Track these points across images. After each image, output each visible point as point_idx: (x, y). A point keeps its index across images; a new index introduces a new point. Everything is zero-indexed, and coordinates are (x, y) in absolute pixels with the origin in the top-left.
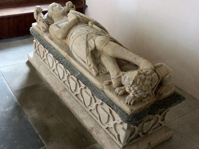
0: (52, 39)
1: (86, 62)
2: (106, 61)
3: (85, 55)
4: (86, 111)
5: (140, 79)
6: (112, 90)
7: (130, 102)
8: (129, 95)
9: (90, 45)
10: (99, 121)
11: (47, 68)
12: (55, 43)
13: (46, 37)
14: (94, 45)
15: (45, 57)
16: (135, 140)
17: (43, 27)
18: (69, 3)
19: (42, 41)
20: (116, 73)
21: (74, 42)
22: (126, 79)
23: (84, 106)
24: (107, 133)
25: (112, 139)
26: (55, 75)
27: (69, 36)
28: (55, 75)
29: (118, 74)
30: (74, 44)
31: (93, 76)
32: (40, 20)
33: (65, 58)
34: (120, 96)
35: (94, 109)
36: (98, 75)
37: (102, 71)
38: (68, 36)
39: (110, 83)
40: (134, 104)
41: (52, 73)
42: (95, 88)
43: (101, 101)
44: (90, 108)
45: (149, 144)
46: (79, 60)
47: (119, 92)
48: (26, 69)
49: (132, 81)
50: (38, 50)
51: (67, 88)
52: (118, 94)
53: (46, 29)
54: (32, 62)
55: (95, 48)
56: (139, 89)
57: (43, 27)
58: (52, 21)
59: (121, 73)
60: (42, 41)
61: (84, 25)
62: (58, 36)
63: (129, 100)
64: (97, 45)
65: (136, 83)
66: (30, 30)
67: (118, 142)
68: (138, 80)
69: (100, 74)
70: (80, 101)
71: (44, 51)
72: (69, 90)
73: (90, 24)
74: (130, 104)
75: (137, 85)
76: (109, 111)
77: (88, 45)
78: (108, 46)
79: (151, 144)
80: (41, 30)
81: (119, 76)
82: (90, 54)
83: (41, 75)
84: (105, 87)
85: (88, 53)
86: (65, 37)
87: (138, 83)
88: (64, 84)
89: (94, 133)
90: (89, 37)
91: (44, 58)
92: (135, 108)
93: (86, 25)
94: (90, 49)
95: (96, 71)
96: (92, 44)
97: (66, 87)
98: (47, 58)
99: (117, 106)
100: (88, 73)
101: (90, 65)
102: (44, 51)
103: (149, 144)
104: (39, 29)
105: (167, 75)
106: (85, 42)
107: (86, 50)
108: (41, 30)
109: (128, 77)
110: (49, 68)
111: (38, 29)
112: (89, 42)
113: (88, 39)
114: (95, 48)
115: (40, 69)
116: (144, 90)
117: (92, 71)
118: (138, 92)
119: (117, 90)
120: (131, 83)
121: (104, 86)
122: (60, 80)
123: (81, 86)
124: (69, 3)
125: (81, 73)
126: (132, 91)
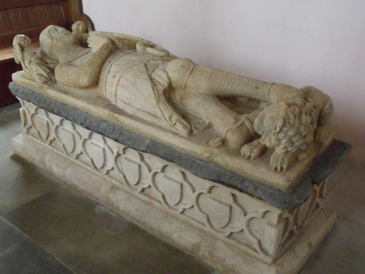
0: (66, 93)
1: (159, 114)
2: (199, 104)
3: (154, 102)
4: (172, 216)
5: (293, 113)
6: (236, 153)
7: (281, 164)
8: (274, 153)
9: (158, 82)
10: (208, 228)
11: (61, 156)
12: (77, 98)
13: (51, 93)
14: (165, 78)
15: (53, 135)
16: (288, 244)
17: (39, 74)
18: (78, 25)
19: (42, 101)
20: (231, 120)
21: (121, 83)
22: (265, 120)
23: (167, 207)
24: (232, 245)
25: (247, 254)
26: (84, 166)
27: (102, 77)
28: (84, 166)
29: (237, 120)
30: (122, 86)
31: (182, 137)
32: (30, 62)
33: (104, 121)
34: (255, 158)
35: (193, 206)
36: (191, 133)
37: (198, 126)
38: (101, 77)
39: (224, 142)
40: (289, 168)
41: (73, 163)
42: (192, 159)
43: (208, 184)
44: (181, 207)
45: (310, 244)
46: (140, 115)
47: (251, 152)
48: (16, 169)
49: (282, 120)
50: (34, 125)
51: (117, 183)
52: (250, 157)
53: (46, 76)
54: (24, 155)
55: (170, 84)
56: (296, 135)
57: (39, 74)
58: (55, 61)
59: (243, 118)
60: (42, 101)
61: (129, 52)
62: (81, 80)
63: (280, 162)
64: (174, 76)
65: (289, 123)
66: (10, 83)
67: (261, 256)
68: (292, 116)
69: (195, 132)
70: (153, 201)
71: (48, 124)
72: (126, 187)
73: (139, 47)
74: (282, 169)
75: (291, 126)
76: (230, 201)
77: (155, 81)
78: (196, 75)
79: (313, 243)
80: (34, 81)
81: (240, 123)
82: (163, 98)
83: (51, 173)
84: (216, 151)
85: (159, 96)
86: (95, 82)
87: (292, 122)
88: (108, 178)
89: (203, 253)
90: (149, 67)
91: (51, 139)
92: (293, 175)
93: (132, 51)
94: (161, 89)
95: (185, 127)
96: (162, 79)
97: (114, 181)
98: (57, 136)
99: (252, 182)
100: (170, 135)
101: (170, 117)
102: (48, 124)
103: (310, 244)
104: (30, 80)
105: (325, 105)
106: (146, 77)
107: (153, 90)
108: (34, 81)
109: (268, 116)
110: (65, 155)
111: (28, 81)
112: (154, 76)
113: (150, 70)
114: (170, 84)
115: (47, 163)
116: (303, 134)
117: (177, 130)
118: (294, 140)
119: (246, 150)
120: (279, 124)
121: (214, 149)
122: (98, 173)
123: (152, 168)
124: (78, 25)
125: (151, 139)
126: (284, 141)
